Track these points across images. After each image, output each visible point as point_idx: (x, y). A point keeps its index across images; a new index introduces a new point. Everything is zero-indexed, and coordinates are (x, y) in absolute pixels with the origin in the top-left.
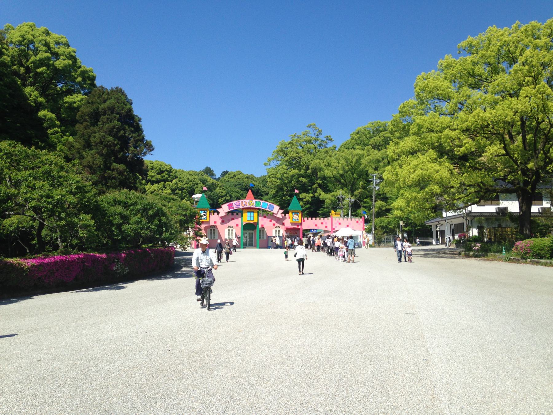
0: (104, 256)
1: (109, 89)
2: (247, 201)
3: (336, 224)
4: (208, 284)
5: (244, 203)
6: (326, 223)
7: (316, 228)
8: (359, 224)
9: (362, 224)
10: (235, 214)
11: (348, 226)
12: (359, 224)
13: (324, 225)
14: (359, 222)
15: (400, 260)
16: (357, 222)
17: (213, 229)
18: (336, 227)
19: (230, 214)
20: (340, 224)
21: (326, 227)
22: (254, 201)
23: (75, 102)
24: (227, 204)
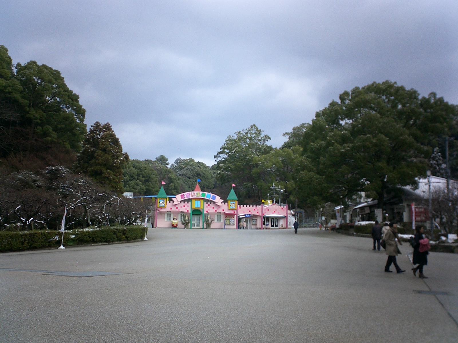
0: (5, 225)
1: (207, 166)
2: (195, 192)
3: (265, 210)
4: (66, 251)
5: (193, 194)
6: (258, 210)
7: (250, 213)
8: (284, 210)
9: (286, 210)
10: (186, 202)
11: (275, 212)
12: (284, 210)
13: (256, 211)
14: (284, 209)
15: (165, 208)
16: (282, 209)
17: (169, 213)
18: (265, 213)
19: (183, 202)
20: (268, 210)
21: (258, 212)
22: (201, 192)
23: (23, 103)
24: (180, 195)
